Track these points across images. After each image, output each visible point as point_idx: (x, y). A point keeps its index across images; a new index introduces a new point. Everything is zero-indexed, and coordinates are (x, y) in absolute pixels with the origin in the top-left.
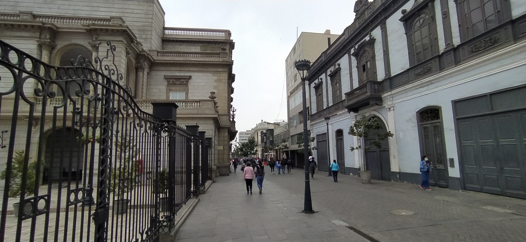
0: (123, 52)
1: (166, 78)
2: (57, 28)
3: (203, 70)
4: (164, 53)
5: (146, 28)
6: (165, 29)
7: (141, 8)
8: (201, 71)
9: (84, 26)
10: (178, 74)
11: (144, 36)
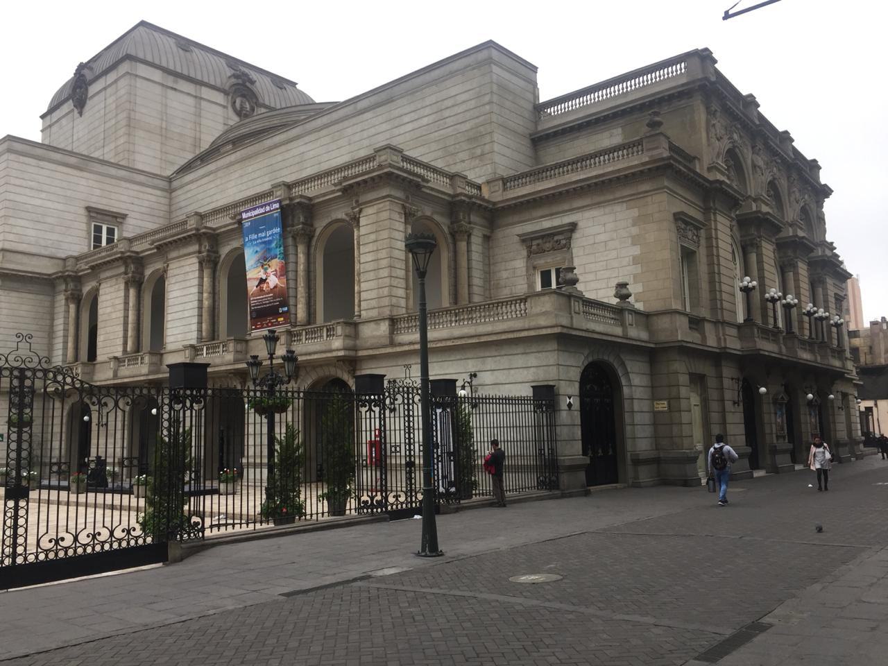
0: (396, 216)
1: (526, 240)
2: (310, 199)
3: (602, 198)
4: (537, 173)
5: (482, 129)
6: (539, 109)
7: (468, 86)
8: (598, 205)
9: (335, 185)
10: (547, 224)
11: (478, 151)
